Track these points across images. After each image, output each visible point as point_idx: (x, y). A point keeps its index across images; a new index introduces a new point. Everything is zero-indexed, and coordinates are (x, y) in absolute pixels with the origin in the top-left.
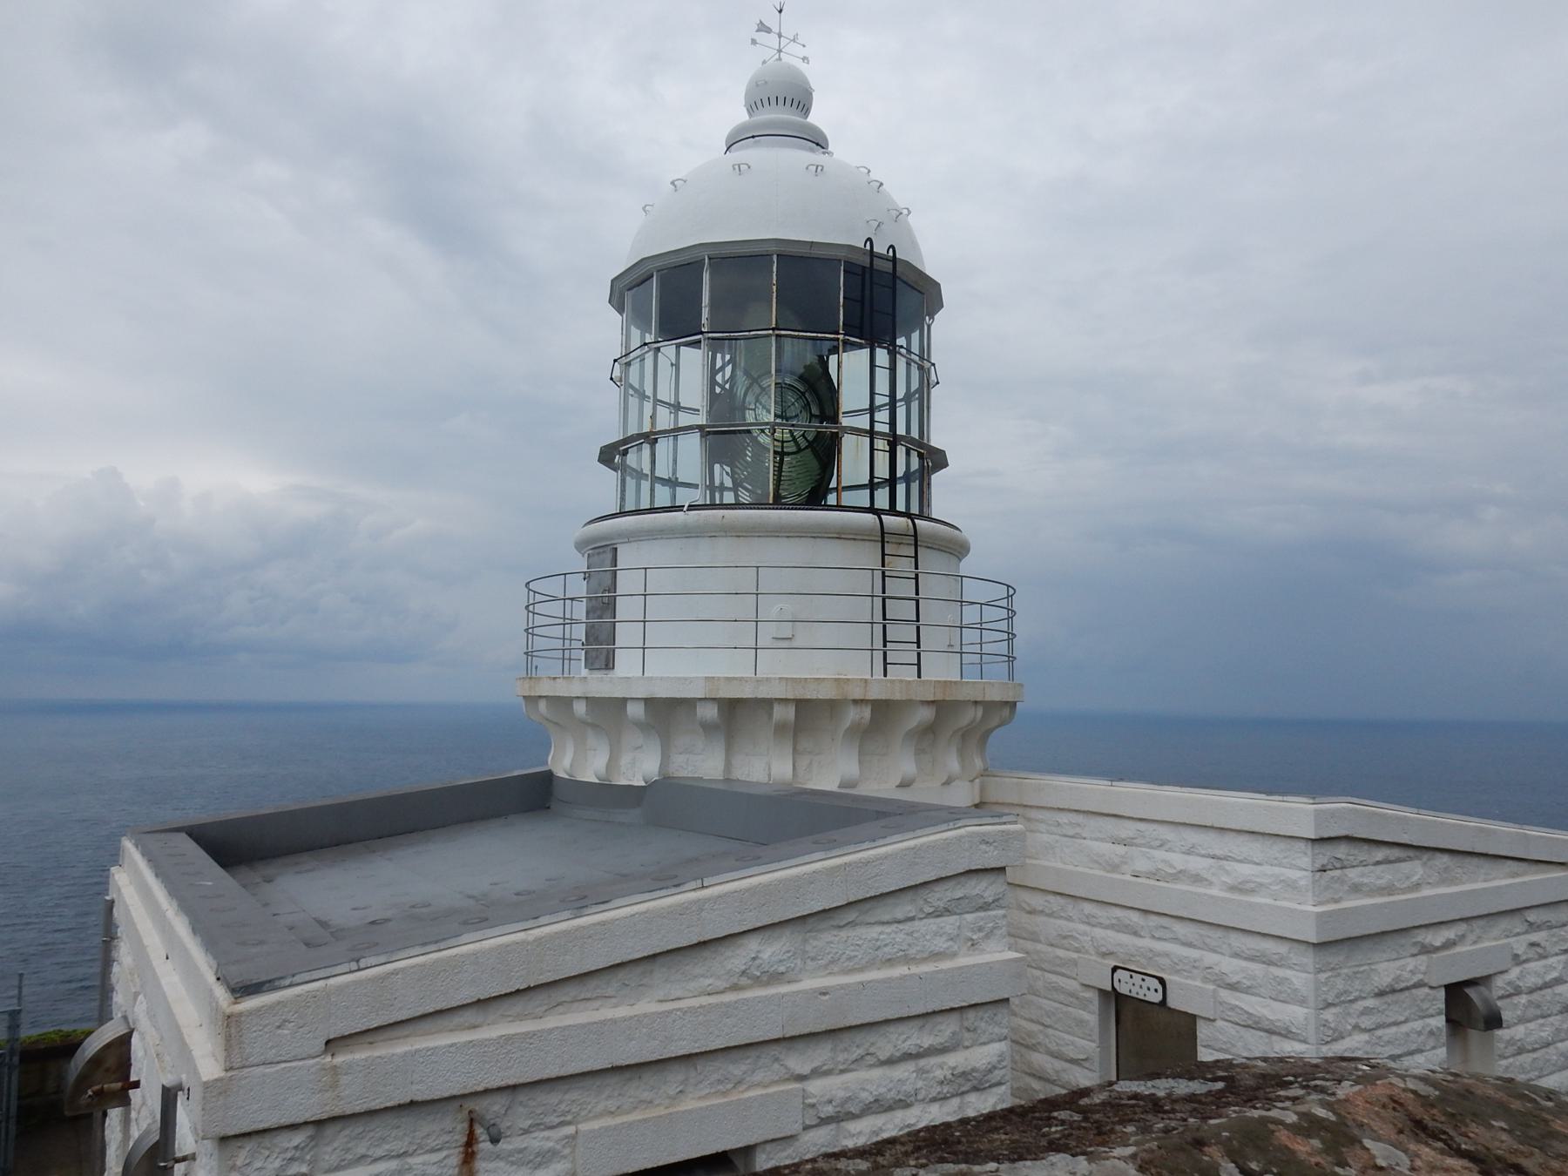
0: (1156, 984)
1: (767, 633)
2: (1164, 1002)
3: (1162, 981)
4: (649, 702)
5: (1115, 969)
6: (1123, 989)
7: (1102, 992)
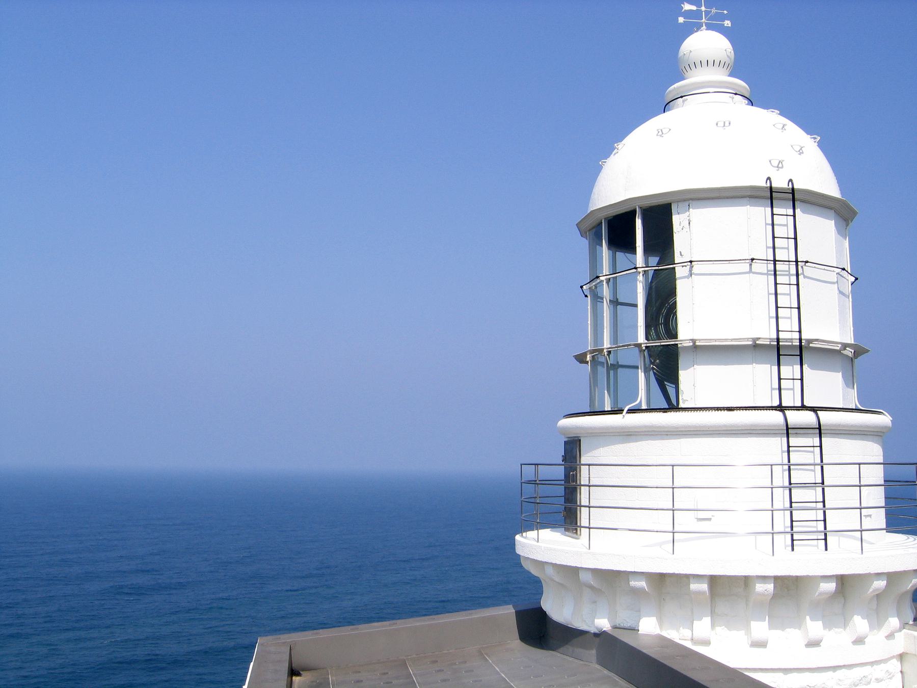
1: (685, 521)
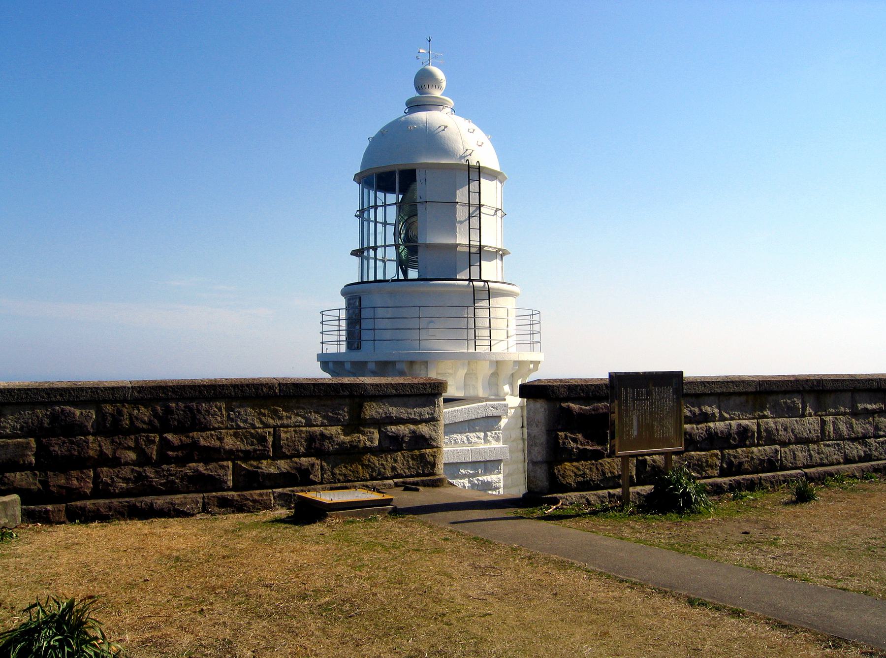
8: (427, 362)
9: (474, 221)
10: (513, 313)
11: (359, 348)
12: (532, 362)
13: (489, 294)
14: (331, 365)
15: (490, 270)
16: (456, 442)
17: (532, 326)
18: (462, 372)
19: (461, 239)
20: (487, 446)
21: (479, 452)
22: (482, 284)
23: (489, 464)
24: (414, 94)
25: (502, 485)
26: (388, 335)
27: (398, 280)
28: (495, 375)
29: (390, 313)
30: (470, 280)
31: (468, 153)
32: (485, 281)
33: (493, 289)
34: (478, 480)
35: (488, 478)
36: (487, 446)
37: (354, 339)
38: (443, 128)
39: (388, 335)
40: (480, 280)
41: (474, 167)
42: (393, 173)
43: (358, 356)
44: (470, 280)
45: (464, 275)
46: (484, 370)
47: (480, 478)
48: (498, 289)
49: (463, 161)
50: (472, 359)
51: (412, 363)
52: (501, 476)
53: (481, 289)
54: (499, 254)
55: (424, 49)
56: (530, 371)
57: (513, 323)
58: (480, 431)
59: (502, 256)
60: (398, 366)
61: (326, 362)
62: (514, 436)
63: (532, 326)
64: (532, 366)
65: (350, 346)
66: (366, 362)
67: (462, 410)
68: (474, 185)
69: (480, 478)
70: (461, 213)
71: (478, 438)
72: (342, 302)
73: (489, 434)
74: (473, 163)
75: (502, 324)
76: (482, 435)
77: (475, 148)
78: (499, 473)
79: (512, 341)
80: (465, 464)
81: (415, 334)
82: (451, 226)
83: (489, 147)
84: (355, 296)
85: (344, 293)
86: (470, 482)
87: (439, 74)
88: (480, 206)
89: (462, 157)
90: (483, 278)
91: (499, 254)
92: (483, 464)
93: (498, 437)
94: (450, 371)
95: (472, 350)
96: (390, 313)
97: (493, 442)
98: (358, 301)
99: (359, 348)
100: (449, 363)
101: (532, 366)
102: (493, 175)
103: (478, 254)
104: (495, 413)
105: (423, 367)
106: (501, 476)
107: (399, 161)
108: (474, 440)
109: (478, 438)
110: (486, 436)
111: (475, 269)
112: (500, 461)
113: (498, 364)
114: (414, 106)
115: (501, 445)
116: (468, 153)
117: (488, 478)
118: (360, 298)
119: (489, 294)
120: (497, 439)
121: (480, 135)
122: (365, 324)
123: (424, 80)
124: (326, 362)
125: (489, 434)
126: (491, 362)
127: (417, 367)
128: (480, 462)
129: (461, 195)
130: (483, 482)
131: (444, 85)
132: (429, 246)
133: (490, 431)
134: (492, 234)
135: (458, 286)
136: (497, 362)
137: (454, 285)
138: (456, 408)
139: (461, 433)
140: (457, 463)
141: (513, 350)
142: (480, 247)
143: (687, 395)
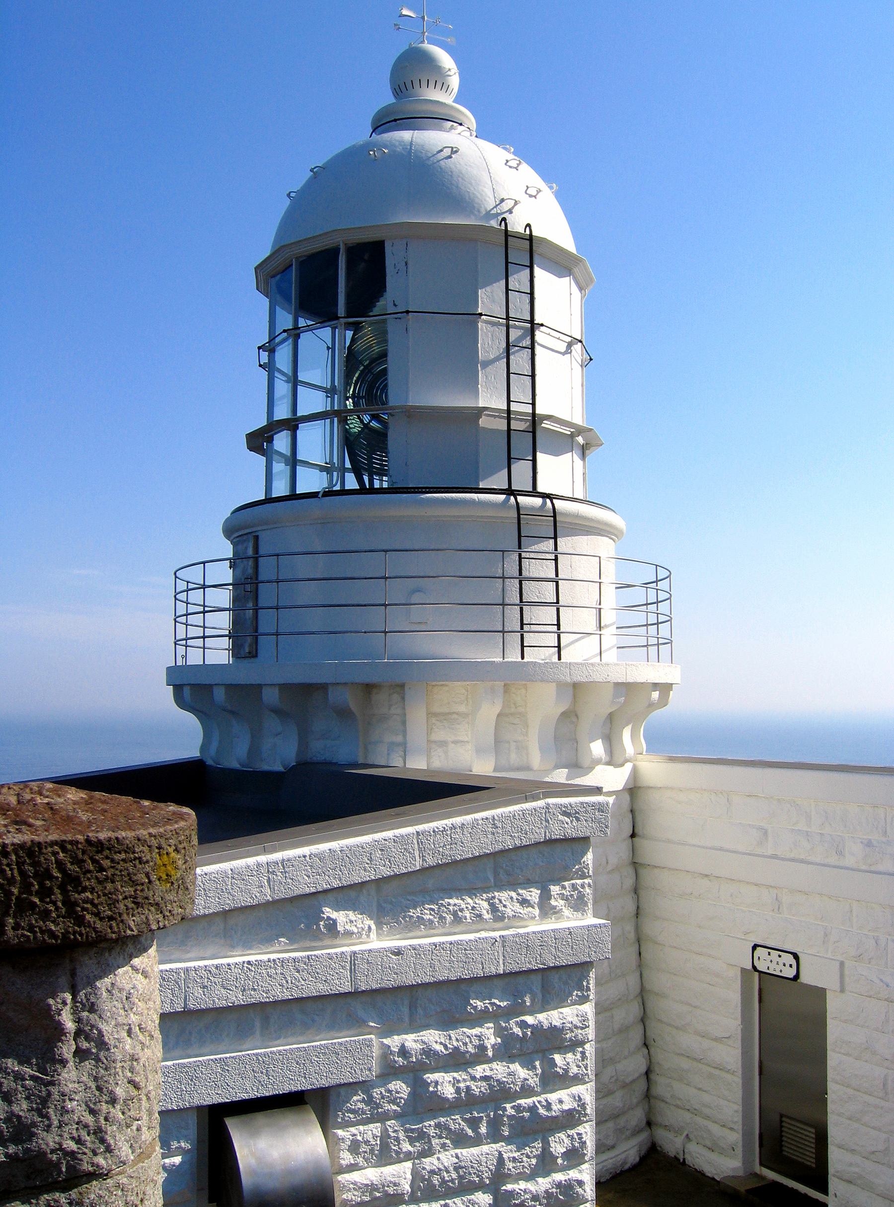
0: (790, 959)
2: (797, 977)
3: (796, 956)
4: (285, 688)
5: (755, 947)
6: (762, 967)
7: (743, 970)
8: (402, 686)
9: (520, 361)
10: (610, 573)
11: (253, 654)
12: (655, 686)
13: (556, 526)
14: (187, 691)
15: (557, 473)
16: (457, 919)
17: (653, 606)
18: (489, 711)
19: (490, 397)
20: (549, 925)
21: (525, 943)
22: (538, 501)
23: (555, 978)
24: (389, 99)
25: (591, 1033)
26: (315, 620)
27: (344, 492)
28: (570, 716)
29: (320, 566)
30: (510, 492)
31: (506, 206)
32: (545, 496)
33: (566, 514)
34: (523, 1025)
35: (552, 1017)
36: (549, 925)
37: (245, 637)
38: (447, 152)
39: (315, 620)
40: (534, 493)
41: (518, 236)
42: (333, 253)
43: (249, 674)
44: (510, 492)
45: (499, 480)
46: (544, 704)
47: (530, 1020)
48: (577, 516)
49: (494, 223)
50: (513, 678)
51: (369, 688)
52: (588, 1008)
53: (536, 513)
54: (578, 441)
55: (410, 9)
56: (652, 706)
57: (610, 598)
58: (528, 883)
59: (584, 451)
60: (335, 696)
61: (192, 688)
62: (613, 861)
63: (653, 606)
64: (655, 695)
65: (237, 651)
66: (260, 686)
67: (474, 824)
68: (519, 279)
69: (530, 1020)
70: (489, 340)
71: (524, 902)
72: (227, 549)
73: (555, 889)
74: (517, 225)
75: (585, 594)
76: (534, 895)
77: (521, 196)
78: (584, 1000)
79: (610, 638)
80: (484, 983)
81: (374, 618)
82: (467, 368)
83: (548, 200)
84: (248, 531)
85: (230, 531)
86: (499, 1031)
87: (446, 60)
88: (533, 326)
89: (489, 215)
90: (540, 489)
91: (578, 441)
92: (537, 979)
93: (581, 897)
94: (462, 709)
95: (514, 656)
96: (320, 566)
97: (567, 912)
98: (251, 545)
99: (253, 654)
100: (459, 688)
101: (655, 695)
102: (563, 264)
103: (529, 435)
104: (571, 828)
105: (396, 697)
106: (588, 1008)
107: (346, 223)
108: (511, 908)
109: (524, 902)
110: (546, 896)
111: (521, 469)
112: (585, 966)
113: (577, 690)
114: (386, 122)
115: (590, 920)
116: (506, 206)
117: (552, 1017)
118: (257, 538)
119: (556, 526)
120: (578, 904)
121: (528, 175)
122: (267, 595)
123: (411, 69)
124: (192, 688)
125: (555, 889)
126: (561, 686)
127: (380, 698)
128: (531, 971)
129: (489, 300)
130: (537, 1029)
131: (455, 81)
132: (413, 414)
133: (557, 881)
134: (560, 390)
135: (481, 503)
136: (576, 686)
137: (472, 502)
138: (458, 820)
139: (472, 891)
140: (460, 981)
141: (610, 656)
142: (535, 419)
143: (257, 613)
